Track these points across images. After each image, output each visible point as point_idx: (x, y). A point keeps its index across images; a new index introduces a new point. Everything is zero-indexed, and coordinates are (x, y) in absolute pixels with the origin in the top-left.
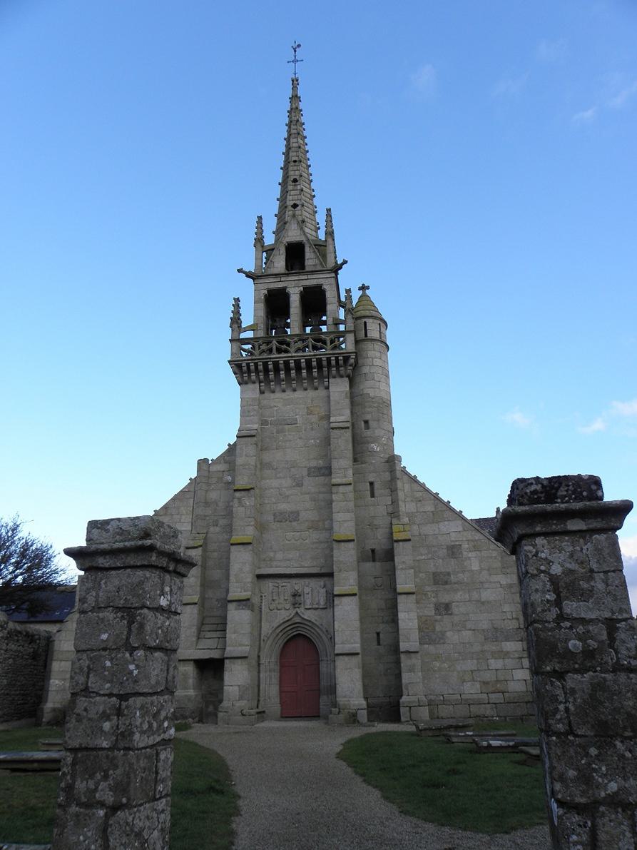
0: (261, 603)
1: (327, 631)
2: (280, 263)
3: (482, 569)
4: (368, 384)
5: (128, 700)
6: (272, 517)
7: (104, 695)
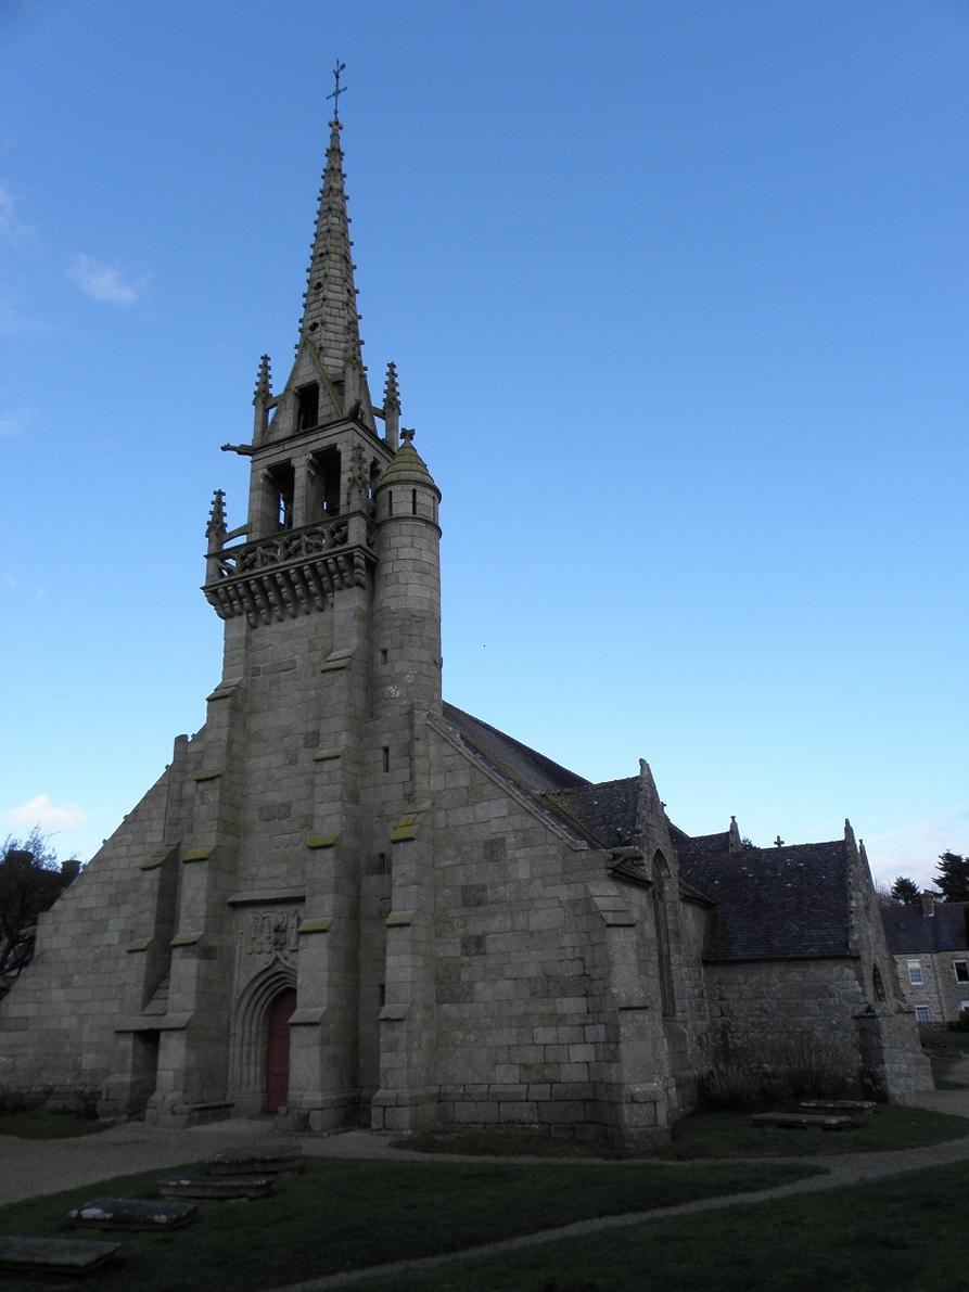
2: (286, 423)
3: (533, 877)
4: (390, 590)
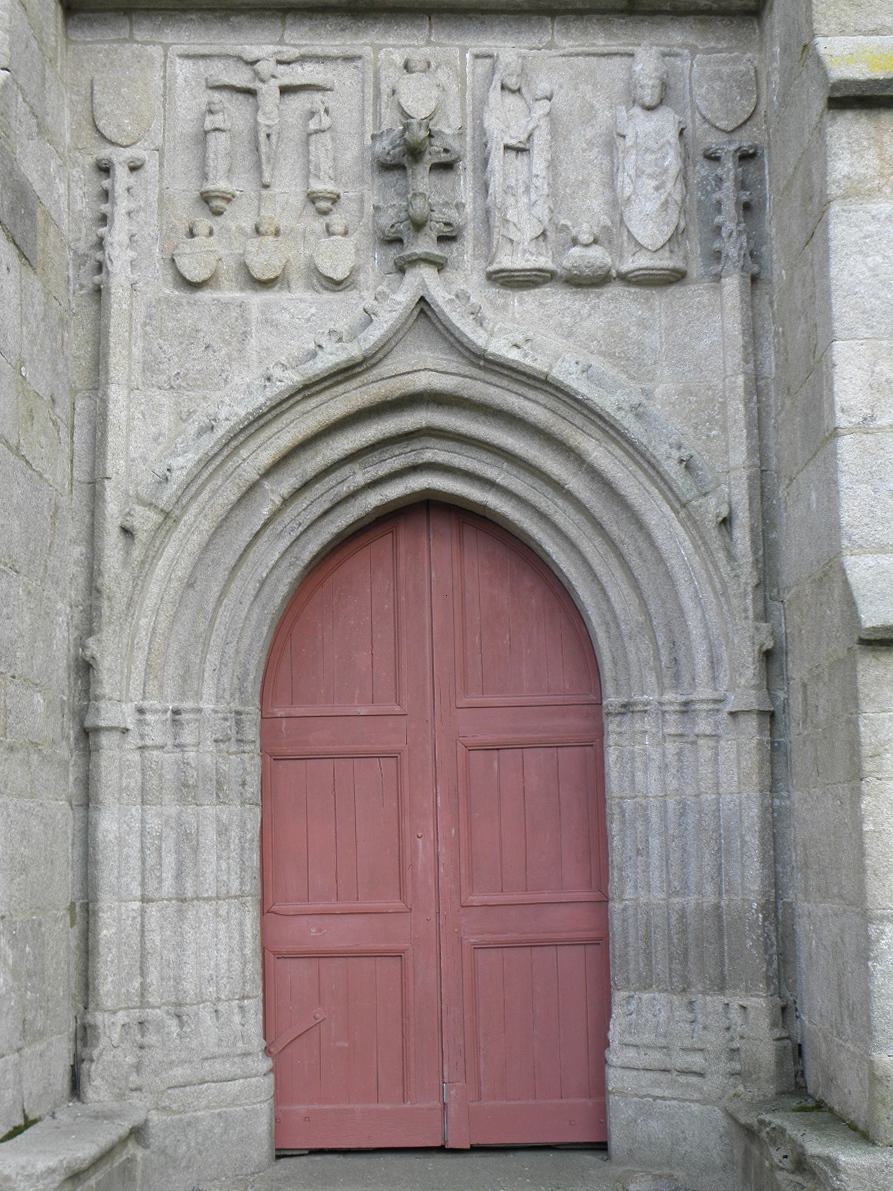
1: (688, 465)
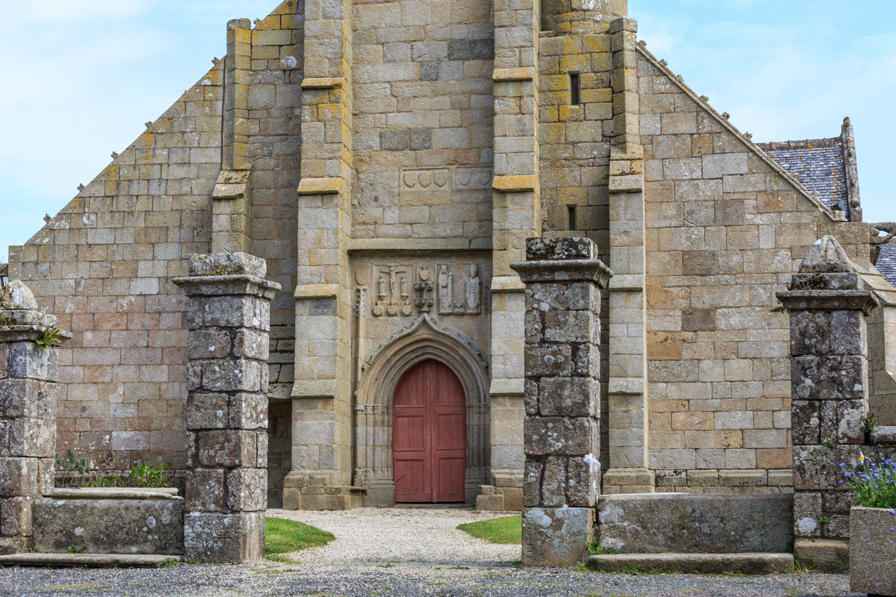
0: (358, 302)
3: (776, 249)
5: (235, 395)
6: (378, 139)
7: (216, 392)
